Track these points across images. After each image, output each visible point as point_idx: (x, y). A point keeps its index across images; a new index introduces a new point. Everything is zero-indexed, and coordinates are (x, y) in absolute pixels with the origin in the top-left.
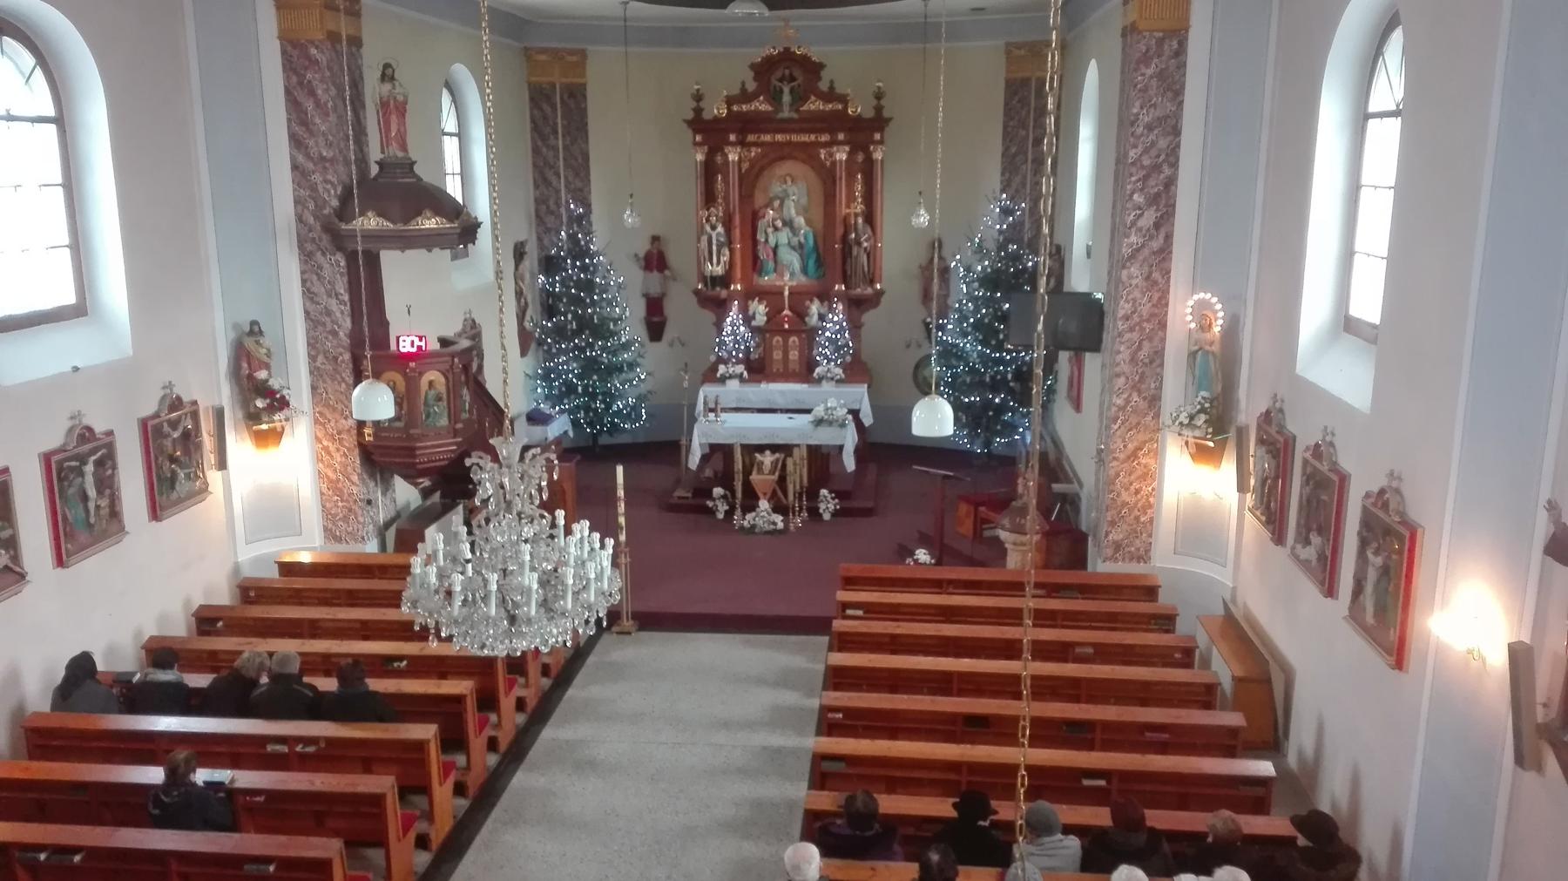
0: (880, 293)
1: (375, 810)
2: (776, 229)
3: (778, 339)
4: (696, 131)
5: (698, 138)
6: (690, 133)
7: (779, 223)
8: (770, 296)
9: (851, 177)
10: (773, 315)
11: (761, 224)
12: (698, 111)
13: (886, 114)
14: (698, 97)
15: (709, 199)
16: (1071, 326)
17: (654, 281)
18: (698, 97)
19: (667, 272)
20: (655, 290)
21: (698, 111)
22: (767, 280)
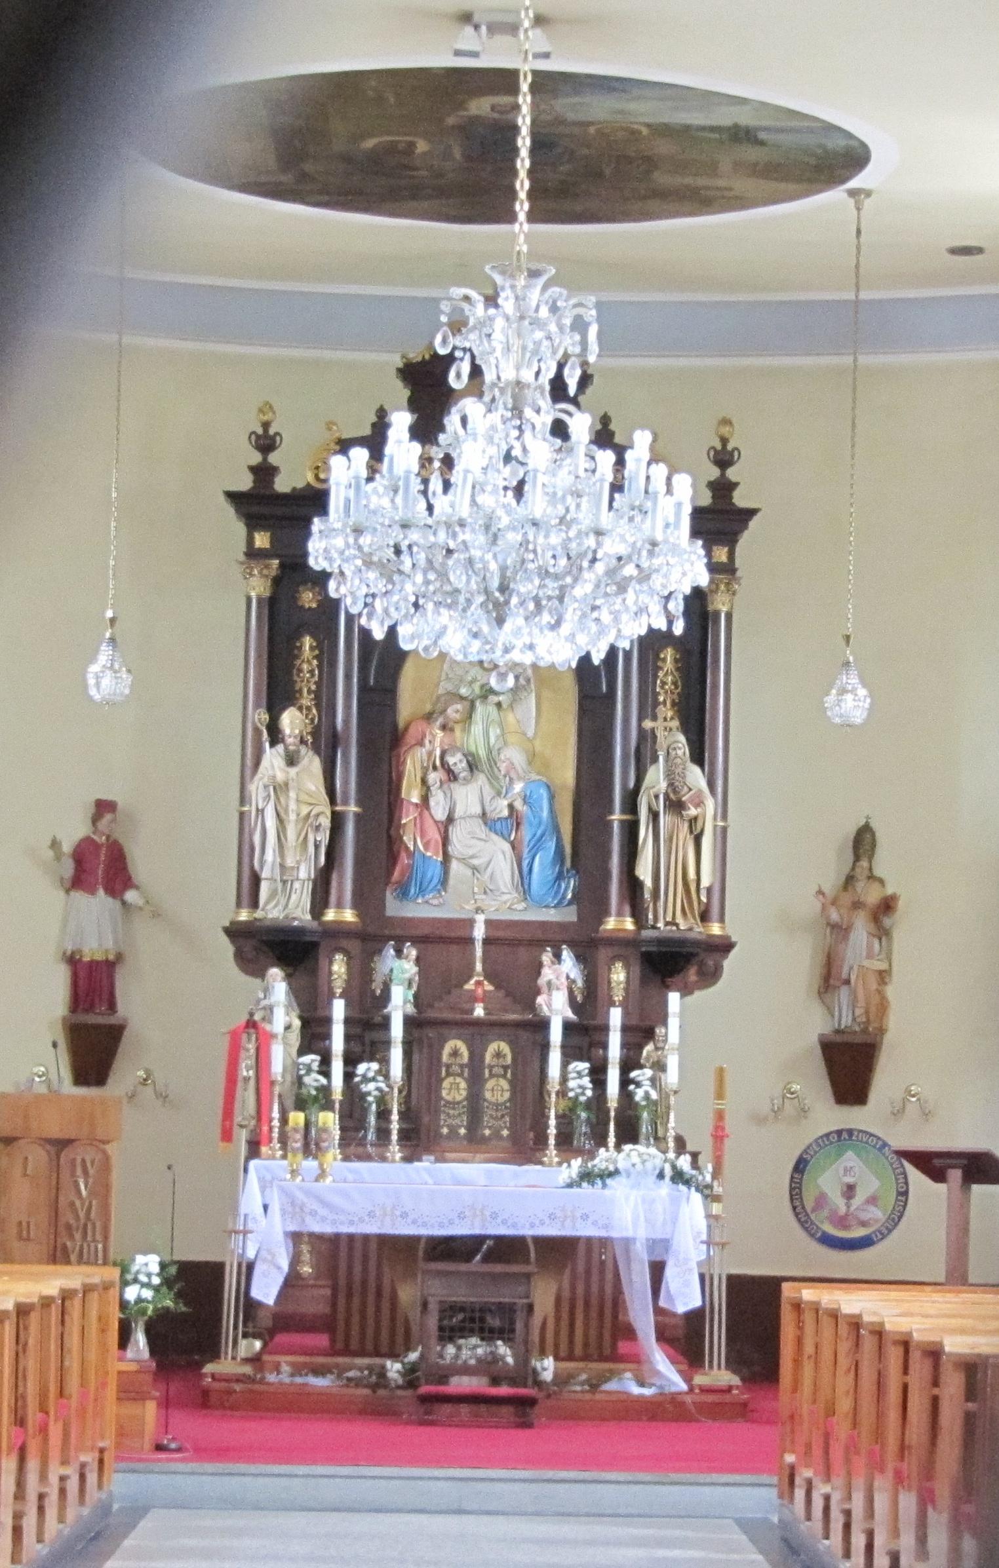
0: (724, 947)
1: (100, 1262)
2: (452, 776)
3: (455, 1047)
4: (253, 522)
5: (262, 540)
6: (239, 528)
7: (456, 761)
8: (441, 942)
9: (345, 793)
10: (436, 987)
11: (412, 764)
12: (263, 473)
13: (740, 499)
14: (266, 443)
15: (278, 692)
16: (697, 801)
17: (93, 922)
18: (266, 443)
19: (131, 896)
20: (94, 949)
21: (263, 473)
22: (420, 909)
